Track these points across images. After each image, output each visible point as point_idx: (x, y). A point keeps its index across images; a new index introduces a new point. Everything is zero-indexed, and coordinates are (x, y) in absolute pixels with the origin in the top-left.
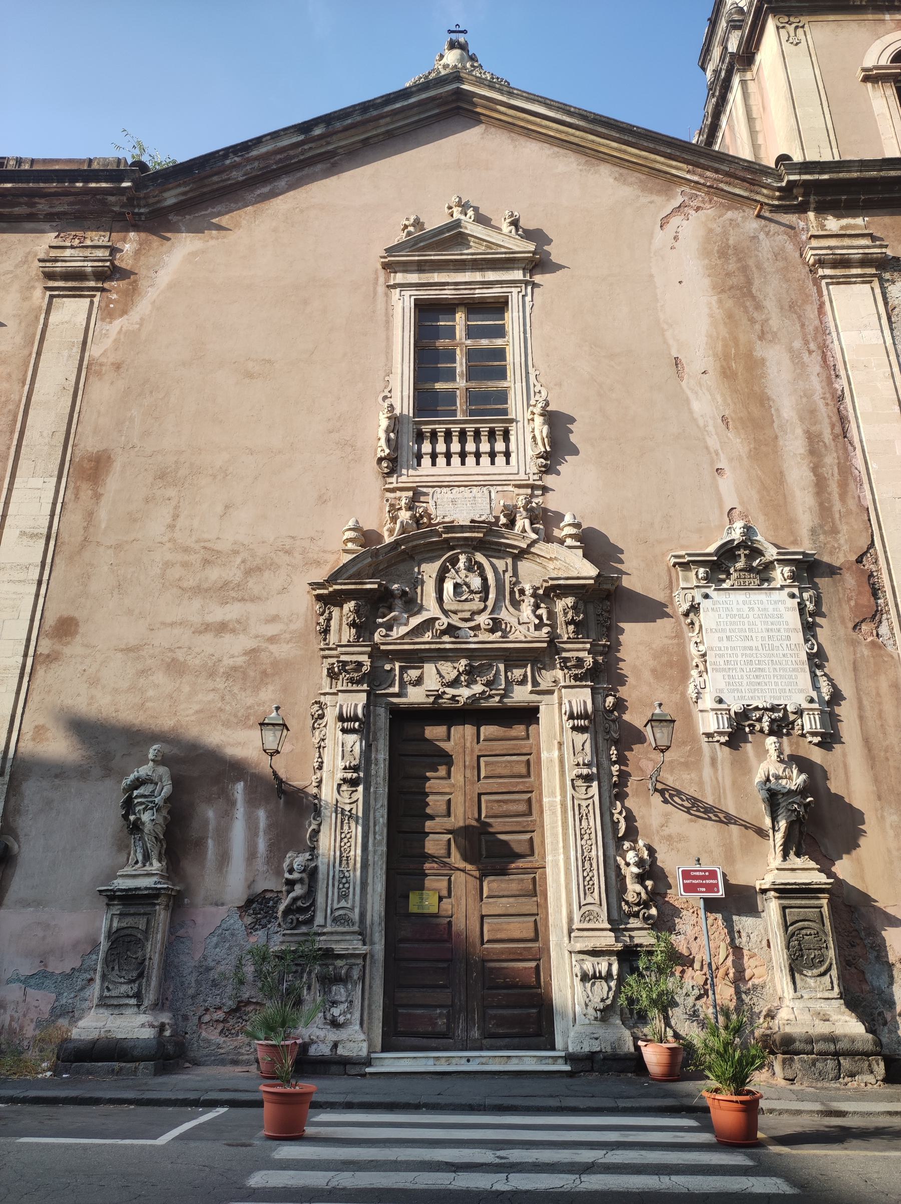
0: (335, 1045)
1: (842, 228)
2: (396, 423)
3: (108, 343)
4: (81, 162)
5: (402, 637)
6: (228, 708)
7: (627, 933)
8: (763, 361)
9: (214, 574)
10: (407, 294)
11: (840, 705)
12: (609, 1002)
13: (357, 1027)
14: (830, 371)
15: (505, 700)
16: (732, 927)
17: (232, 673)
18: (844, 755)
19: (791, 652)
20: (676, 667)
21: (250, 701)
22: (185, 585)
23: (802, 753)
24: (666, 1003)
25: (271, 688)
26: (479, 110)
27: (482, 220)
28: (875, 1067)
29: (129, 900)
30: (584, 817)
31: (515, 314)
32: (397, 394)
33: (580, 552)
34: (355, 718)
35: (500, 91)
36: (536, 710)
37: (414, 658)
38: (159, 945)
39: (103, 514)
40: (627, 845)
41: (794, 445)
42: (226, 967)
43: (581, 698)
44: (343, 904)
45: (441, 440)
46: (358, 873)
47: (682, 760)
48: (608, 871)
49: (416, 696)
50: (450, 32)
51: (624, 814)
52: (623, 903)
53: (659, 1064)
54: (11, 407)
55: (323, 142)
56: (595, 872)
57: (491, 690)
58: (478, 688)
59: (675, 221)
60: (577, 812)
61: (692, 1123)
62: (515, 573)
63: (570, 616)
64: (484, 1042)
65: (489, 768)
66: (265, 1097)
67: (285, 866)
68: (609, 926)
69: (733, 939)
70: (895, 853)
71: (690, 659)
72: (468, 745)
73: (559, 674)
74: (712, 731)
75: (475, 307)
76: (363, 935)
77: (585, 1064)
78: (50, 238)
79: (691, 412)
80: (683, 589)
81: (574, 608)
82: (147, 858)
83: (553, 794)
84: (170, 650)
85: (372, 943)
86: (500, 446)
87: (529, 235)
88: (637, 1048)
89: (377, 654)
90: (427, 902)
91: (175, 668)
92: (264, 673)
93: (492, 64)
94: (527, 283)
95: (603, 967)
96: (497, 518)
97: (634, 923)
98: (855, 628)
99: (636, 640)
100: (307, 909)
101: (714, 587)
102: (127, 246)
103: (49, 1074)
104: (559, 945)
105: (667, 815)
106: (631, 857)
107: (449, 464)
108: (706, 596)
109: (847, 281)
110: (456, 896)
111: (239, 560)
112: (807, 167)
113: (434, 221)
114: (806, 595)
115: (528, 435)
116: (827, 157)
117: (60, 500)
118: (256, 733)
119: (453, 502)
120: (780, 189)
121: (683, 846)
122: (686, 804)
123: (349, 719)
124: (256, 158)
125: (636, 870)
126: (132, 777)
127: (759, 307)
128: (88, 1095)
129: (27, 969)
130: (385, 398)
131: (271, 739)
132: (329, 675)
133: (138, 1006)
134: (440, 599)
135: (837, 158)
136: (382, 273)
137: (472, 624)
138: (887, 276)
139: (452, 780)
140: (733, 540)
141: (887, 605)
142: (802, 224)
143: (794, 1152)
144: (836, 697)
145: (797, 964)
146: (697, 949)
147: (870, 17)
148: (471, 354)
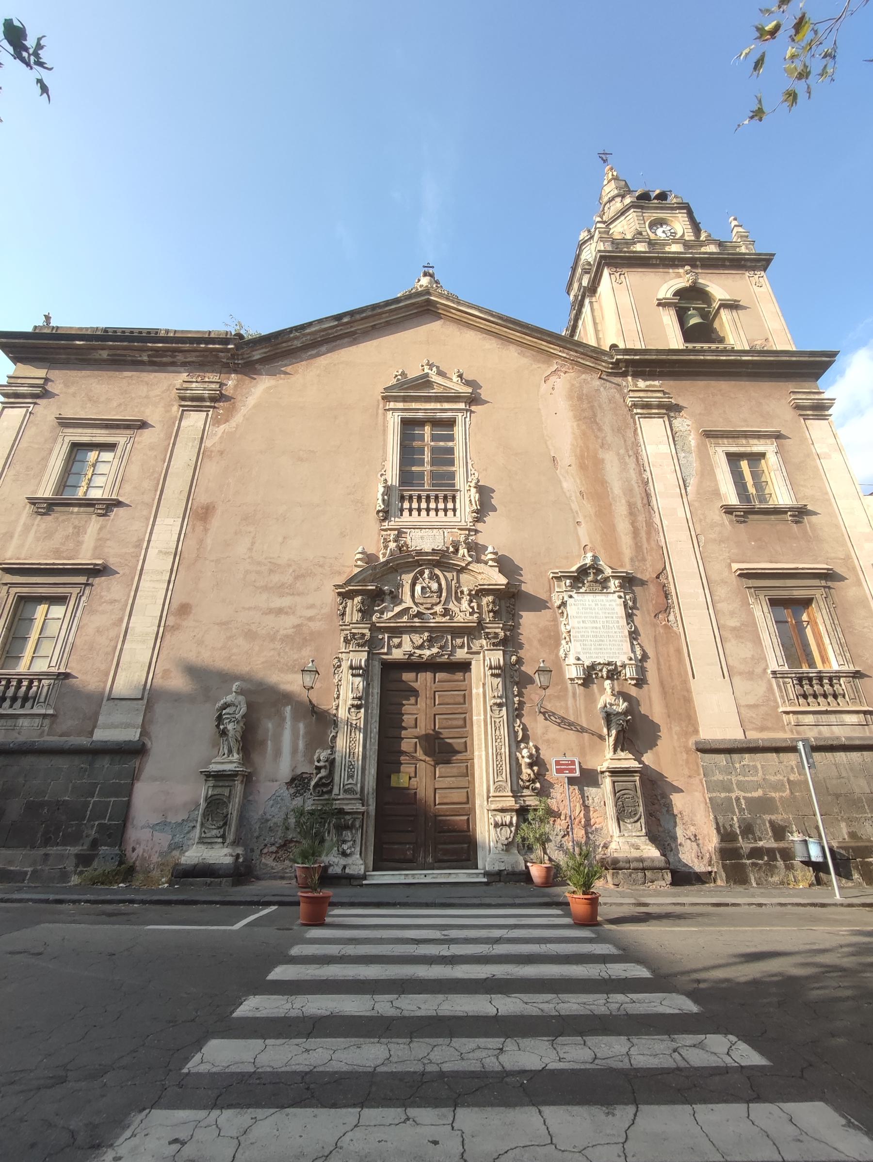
0: (344, 867)
1: (647, 386)
2: (388, 490)
3: (216, 439)
4: (204, 332)
5: (390, 619)
6: (282, 660)
8: (603, 460)
9: (276, 578)
10: (396, 414)
12: (510, 840)
13: (358, 856)
14: (641, 468)
17: (286, 639)
18: (649, 691)
20: (553, 638)
21: (296, 657)
22: (258, 584)
23: (625, 690)
24: (544, 840)
25: (309, 648)
26: (440, 311)
27: (441, 373)
28: (666, 876)
29: (218, 777)
31: (460, 428)
32: (389, 473)
33: (497, 569)
34: (360, 668)
35: (452, 301)
36: (469, 664)
37: (396, 632)
38: (237, 805)
39: (209, 541)
40: (522, 745)
41: (621, 509)
42: (278, 819)
43: (497, 657)
44: (350, 781)
45: (415, 501)
46: (360, 762)
49: (397, 654)
50: (424, 267)
53: (540, 877)
54: (156, 475)
55: (348, 326)
58: (435, 650)
59: (553, 379)
61: (559, 912)
62: (458, 581)
63: (490, 607)
64: (436, 865)
66: (301, 899)
67: (315, 757)
69: (584, 802)
72: (428, 684)
73: (484, 642)
74: (573, 677)
75: (436, 423)
76: (363, 800)
77: (496, 877)
78: (184, 376)
79: (562, 488)
81: (493, 602)
82: (230, 752)
83: (479, 714)
84: (248, 624)
85: (368, 805)
86: (450, 505)
87: (468, 383)
88: (527, 867)
89: (374, 628)
90: (402, 780)
91: (250, 635)
92: (305, 639)
93: (448, 285)
94: (467, 410)
95: (507, 819)
96: (448, 548)
97: (526, 792)
99: (529, 621)
100: (328, 784)
102: (230, 382)
103: (166, 885)
104: (481, 806)
105: (546, 727)
106: (525, 752)
107: (419, 515)
108: (571, 597)
109: (649, 416)
110: (419, 777)
111: (291, 571)
112: (627, 351)
113: (413, 373)
114: (628, 597)
115: (467, 499)
116: (638, 346)
117: (183, 532)
118: (299, 677)
119: (422, 538)
120: (612, 363)
121: (557, 747)
122: (558, 720)
123: (356, 668)
124: (309, 334)
125: (528, 760)
126: (222, 702)
127: (600, 429)
128: (190, 899)
129: (155, 819)
130: (382, 475)
131: (308, 679)
132: (344, 641)
133: (223, 843)
134: (413, 596)
135: (644, 347)
136: (381, 402)
137: (432, 611)
138: (672, 414)
139: (419, 706)
142: (624, 383)
143: (619, 928)
144: (645, 657)
145: (621, 816)
147: (661, 270)
148: (433, 450)
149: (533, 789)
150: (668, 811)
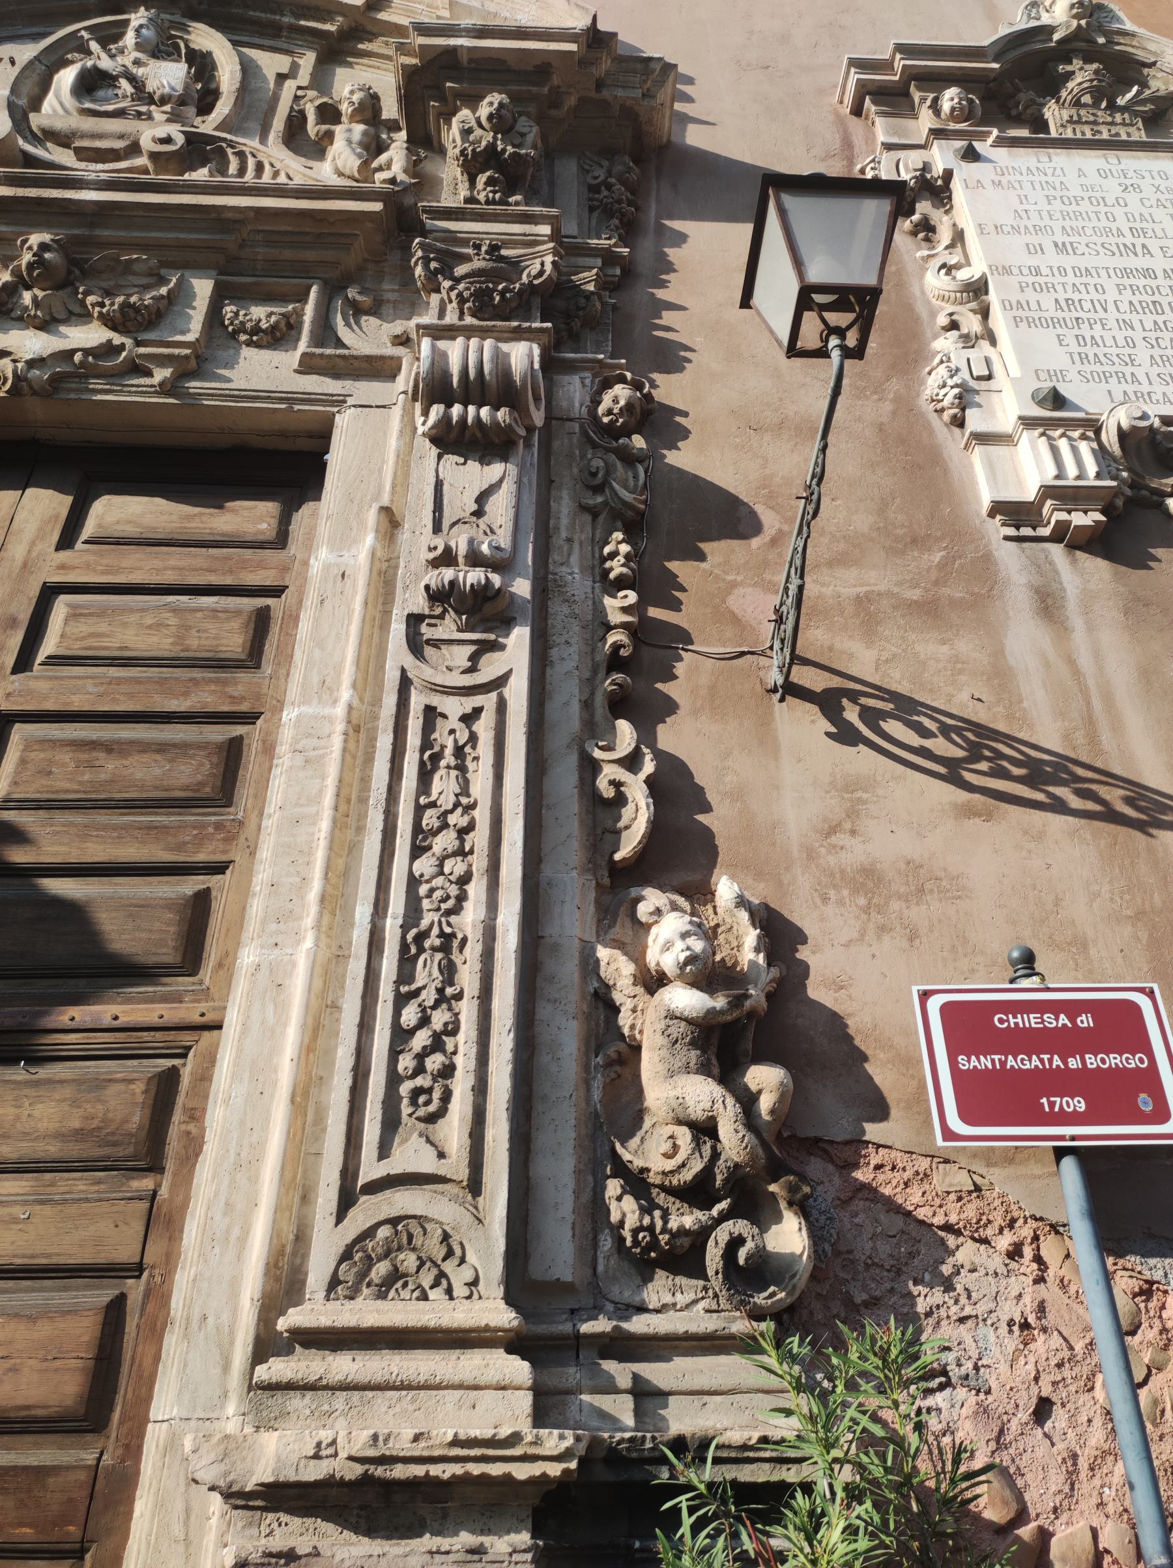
7: (620, 1372)
15: (194, 385)
30: (449, 758)
36: (323, 435)
47: (915, 594)
48: (544, 1011)
51: (649, 767)
52: (613, 1187)
56: (467, 1010)
57: (139, 344)
58: (87, 335)
60: (413, 739)
65: (83, 627)
68: (503, 1317)
71: (924, 315)
74: (1030, 494)
80: (889, 147)
97: (674, 1305)
101: (995, 132)
105: (853, 801)
108: (971, 155)
122: (939, 745)
125: (686, 999)
140: (1049, 30)
146: (1057, 1480)
149: (749, 1274)
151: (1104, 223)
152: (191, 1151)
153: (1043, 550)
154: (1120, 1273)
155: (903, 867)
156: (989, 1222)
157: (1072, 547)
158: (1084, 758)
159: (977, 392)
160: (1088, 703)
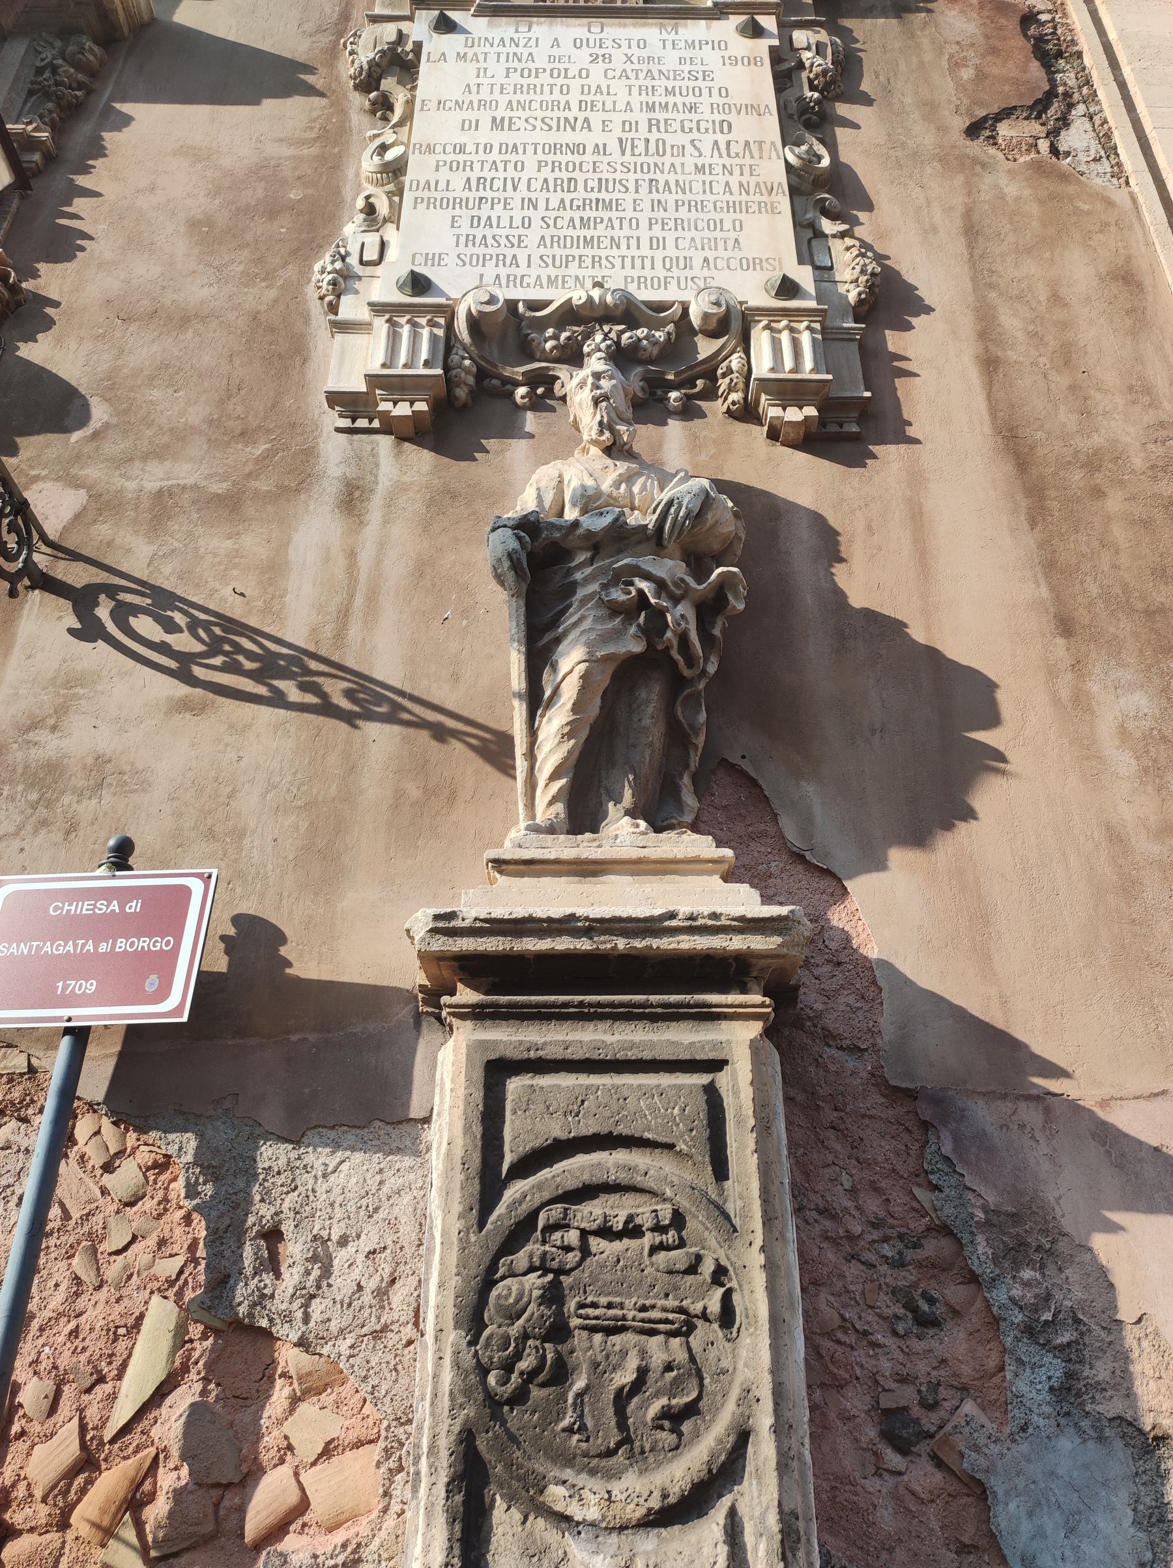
11: (909, 327)
16: (238, 1204)
18: (916, 478)
19: (727, 161)
47: (220, 488)
69: (221, 1282)
70: (1147, 847)
98: (973, 131)
108: (445, 26)
122: (183, 642)
141: (1088, 82)
150: (1069, 1393)
151: (556, 95)
152: (800, 1097)
153: (372, 442)
154: (142, 1148)
155: (90, 761)
156: (32, 1101)
157: (402, 438)
158: (323, 652)
159: (359, 278)
160: (351, 596)
